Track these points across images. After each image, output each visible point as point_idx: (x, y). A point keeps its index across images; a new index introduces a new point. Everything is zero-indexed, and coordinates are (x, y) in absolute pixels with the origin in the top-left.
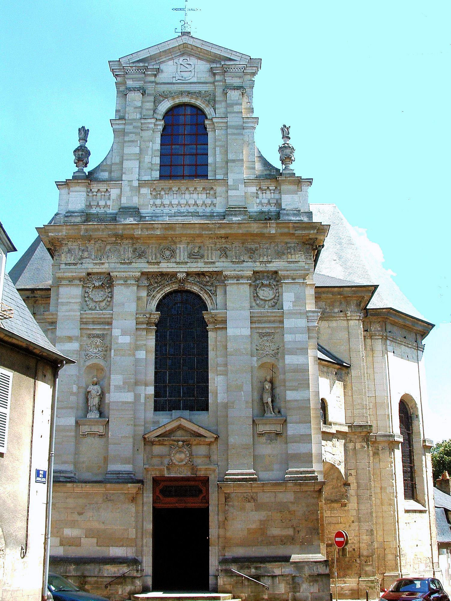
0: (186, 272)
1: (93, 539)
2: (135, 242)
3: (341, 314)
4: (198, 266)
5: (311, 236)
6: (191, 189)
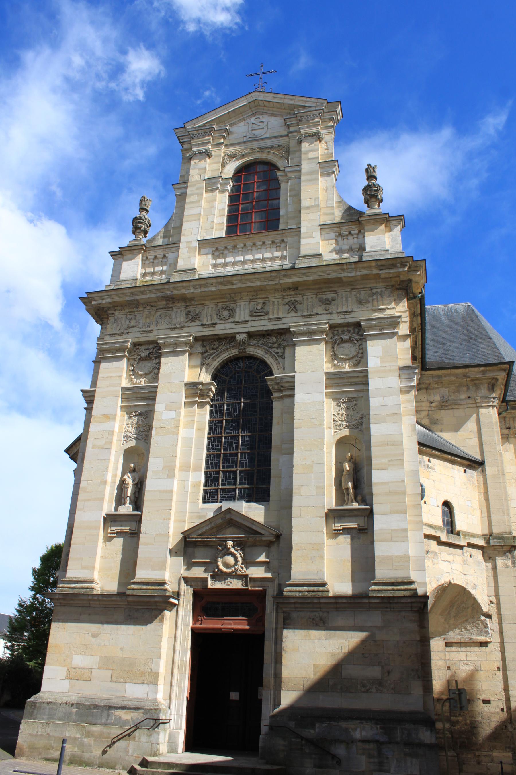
0: (246, 332)
1: (107, 671)
2: (188, 304)
3: (470, 401)
4: (261, 325)
5: (402, 278)
6: (259, 243)
